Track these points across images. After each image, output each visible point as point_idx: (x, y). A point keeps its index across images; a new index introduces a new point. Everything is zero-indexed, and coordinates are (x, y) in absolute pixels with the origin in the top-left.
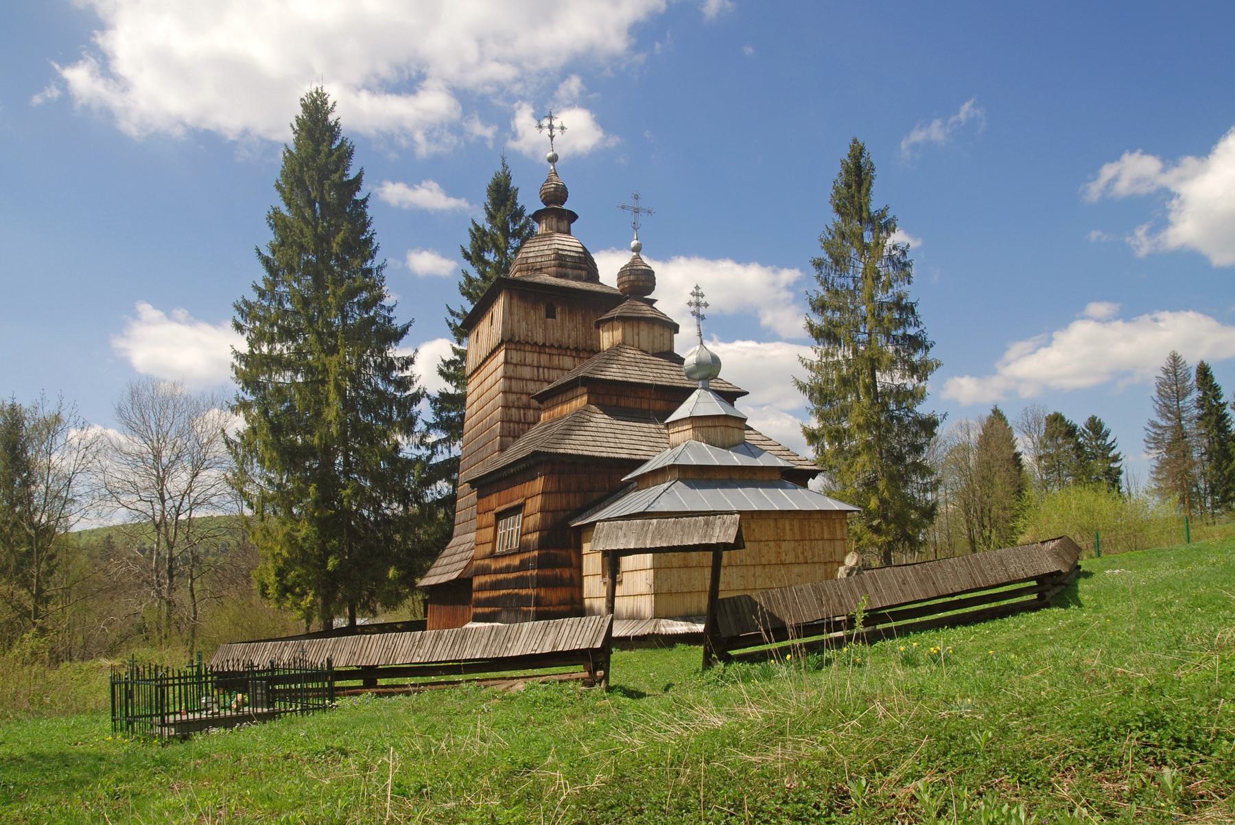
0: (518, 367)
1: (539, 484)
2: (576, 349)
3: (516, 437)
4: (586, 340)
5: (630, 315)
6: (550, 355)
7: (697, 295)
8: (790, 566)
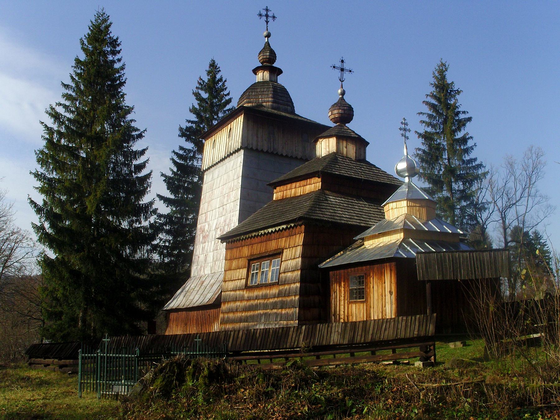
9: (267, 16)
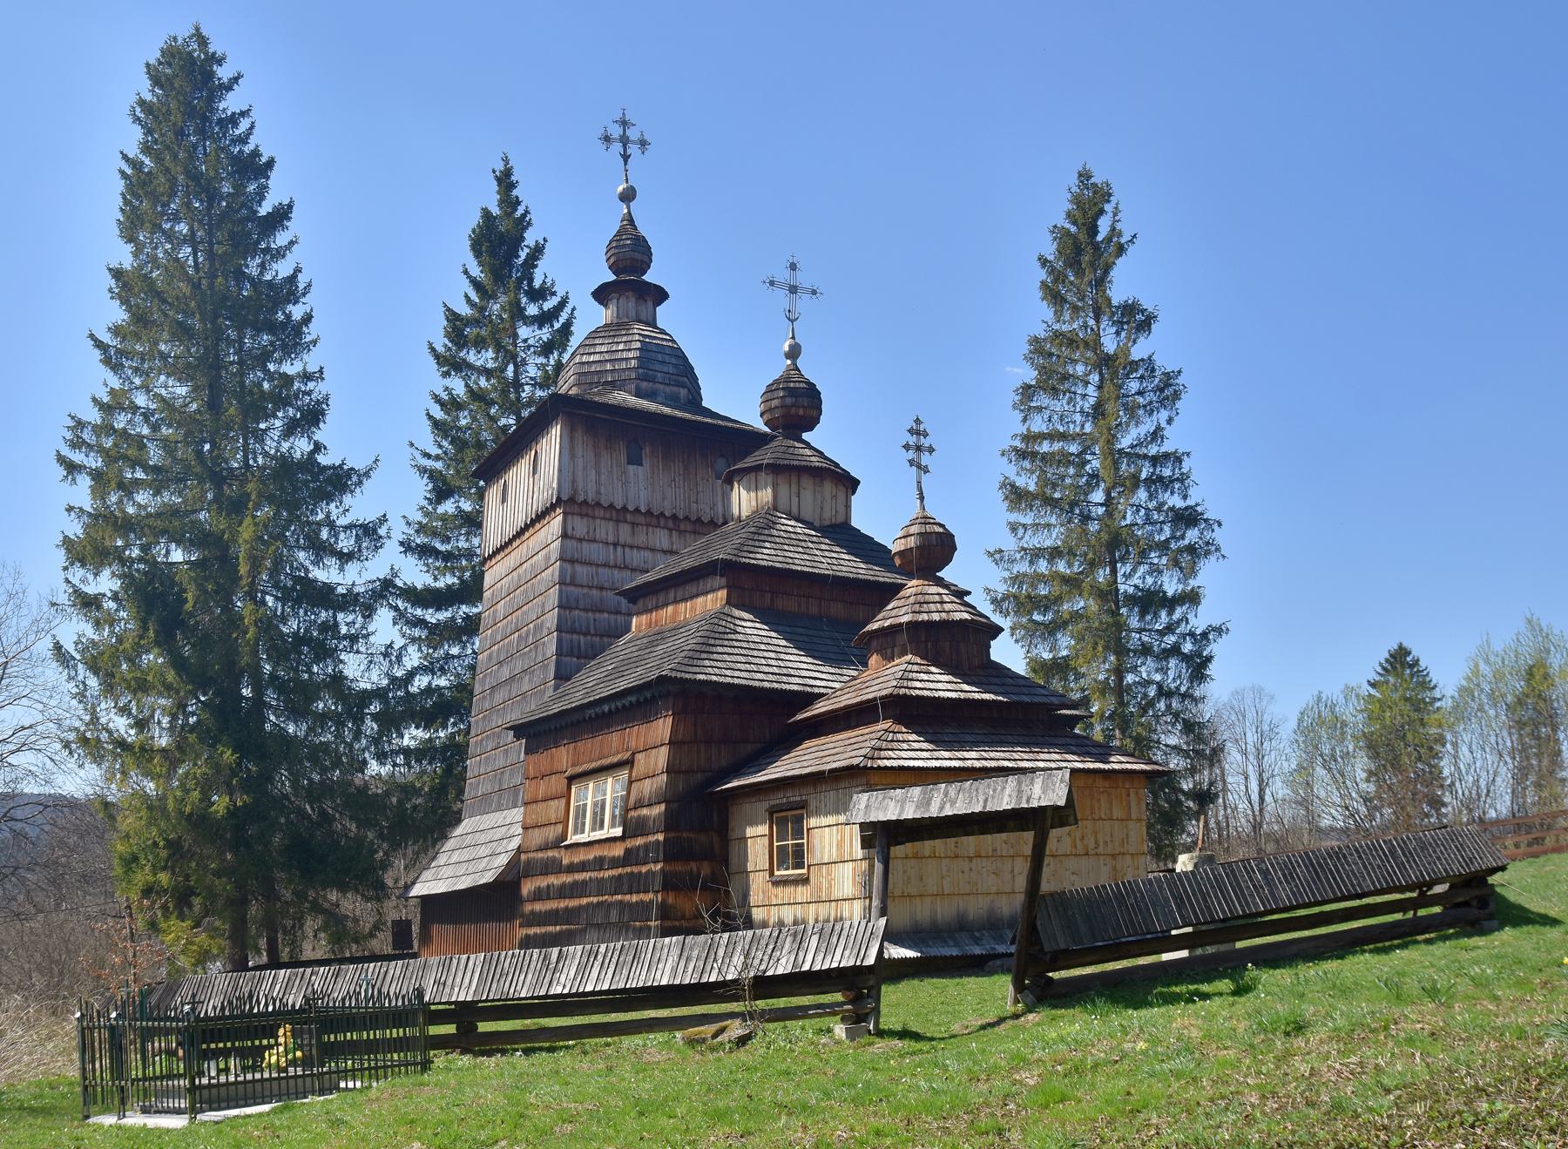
0: (584, 543)
1: (662, 727)
2: (674, 517)
3: (592, 653)
4: (689, 504)
5: (786, 462)
6: (633, 524)
7: (918, 433)
8: (1063, 858)
9: (625, 141)
